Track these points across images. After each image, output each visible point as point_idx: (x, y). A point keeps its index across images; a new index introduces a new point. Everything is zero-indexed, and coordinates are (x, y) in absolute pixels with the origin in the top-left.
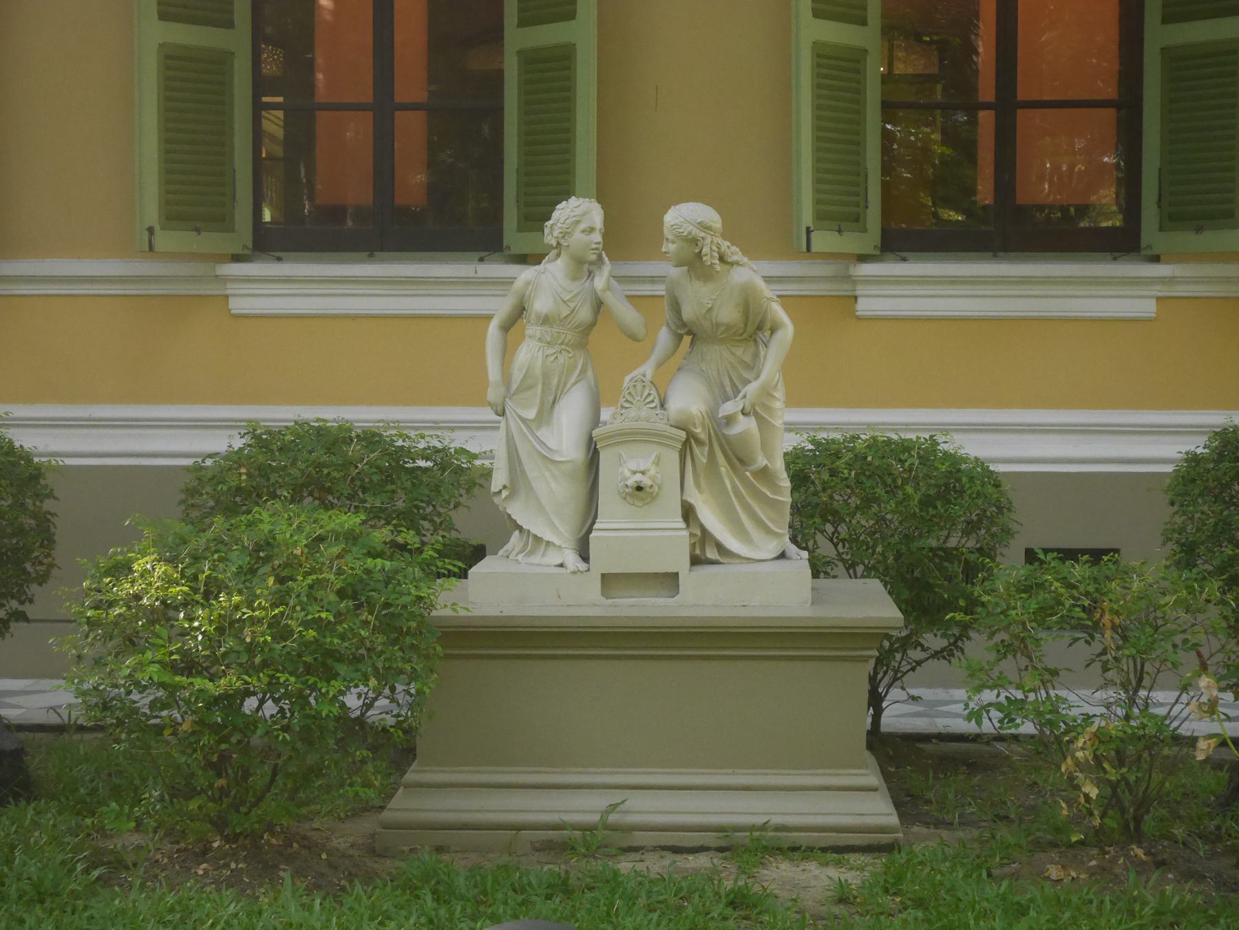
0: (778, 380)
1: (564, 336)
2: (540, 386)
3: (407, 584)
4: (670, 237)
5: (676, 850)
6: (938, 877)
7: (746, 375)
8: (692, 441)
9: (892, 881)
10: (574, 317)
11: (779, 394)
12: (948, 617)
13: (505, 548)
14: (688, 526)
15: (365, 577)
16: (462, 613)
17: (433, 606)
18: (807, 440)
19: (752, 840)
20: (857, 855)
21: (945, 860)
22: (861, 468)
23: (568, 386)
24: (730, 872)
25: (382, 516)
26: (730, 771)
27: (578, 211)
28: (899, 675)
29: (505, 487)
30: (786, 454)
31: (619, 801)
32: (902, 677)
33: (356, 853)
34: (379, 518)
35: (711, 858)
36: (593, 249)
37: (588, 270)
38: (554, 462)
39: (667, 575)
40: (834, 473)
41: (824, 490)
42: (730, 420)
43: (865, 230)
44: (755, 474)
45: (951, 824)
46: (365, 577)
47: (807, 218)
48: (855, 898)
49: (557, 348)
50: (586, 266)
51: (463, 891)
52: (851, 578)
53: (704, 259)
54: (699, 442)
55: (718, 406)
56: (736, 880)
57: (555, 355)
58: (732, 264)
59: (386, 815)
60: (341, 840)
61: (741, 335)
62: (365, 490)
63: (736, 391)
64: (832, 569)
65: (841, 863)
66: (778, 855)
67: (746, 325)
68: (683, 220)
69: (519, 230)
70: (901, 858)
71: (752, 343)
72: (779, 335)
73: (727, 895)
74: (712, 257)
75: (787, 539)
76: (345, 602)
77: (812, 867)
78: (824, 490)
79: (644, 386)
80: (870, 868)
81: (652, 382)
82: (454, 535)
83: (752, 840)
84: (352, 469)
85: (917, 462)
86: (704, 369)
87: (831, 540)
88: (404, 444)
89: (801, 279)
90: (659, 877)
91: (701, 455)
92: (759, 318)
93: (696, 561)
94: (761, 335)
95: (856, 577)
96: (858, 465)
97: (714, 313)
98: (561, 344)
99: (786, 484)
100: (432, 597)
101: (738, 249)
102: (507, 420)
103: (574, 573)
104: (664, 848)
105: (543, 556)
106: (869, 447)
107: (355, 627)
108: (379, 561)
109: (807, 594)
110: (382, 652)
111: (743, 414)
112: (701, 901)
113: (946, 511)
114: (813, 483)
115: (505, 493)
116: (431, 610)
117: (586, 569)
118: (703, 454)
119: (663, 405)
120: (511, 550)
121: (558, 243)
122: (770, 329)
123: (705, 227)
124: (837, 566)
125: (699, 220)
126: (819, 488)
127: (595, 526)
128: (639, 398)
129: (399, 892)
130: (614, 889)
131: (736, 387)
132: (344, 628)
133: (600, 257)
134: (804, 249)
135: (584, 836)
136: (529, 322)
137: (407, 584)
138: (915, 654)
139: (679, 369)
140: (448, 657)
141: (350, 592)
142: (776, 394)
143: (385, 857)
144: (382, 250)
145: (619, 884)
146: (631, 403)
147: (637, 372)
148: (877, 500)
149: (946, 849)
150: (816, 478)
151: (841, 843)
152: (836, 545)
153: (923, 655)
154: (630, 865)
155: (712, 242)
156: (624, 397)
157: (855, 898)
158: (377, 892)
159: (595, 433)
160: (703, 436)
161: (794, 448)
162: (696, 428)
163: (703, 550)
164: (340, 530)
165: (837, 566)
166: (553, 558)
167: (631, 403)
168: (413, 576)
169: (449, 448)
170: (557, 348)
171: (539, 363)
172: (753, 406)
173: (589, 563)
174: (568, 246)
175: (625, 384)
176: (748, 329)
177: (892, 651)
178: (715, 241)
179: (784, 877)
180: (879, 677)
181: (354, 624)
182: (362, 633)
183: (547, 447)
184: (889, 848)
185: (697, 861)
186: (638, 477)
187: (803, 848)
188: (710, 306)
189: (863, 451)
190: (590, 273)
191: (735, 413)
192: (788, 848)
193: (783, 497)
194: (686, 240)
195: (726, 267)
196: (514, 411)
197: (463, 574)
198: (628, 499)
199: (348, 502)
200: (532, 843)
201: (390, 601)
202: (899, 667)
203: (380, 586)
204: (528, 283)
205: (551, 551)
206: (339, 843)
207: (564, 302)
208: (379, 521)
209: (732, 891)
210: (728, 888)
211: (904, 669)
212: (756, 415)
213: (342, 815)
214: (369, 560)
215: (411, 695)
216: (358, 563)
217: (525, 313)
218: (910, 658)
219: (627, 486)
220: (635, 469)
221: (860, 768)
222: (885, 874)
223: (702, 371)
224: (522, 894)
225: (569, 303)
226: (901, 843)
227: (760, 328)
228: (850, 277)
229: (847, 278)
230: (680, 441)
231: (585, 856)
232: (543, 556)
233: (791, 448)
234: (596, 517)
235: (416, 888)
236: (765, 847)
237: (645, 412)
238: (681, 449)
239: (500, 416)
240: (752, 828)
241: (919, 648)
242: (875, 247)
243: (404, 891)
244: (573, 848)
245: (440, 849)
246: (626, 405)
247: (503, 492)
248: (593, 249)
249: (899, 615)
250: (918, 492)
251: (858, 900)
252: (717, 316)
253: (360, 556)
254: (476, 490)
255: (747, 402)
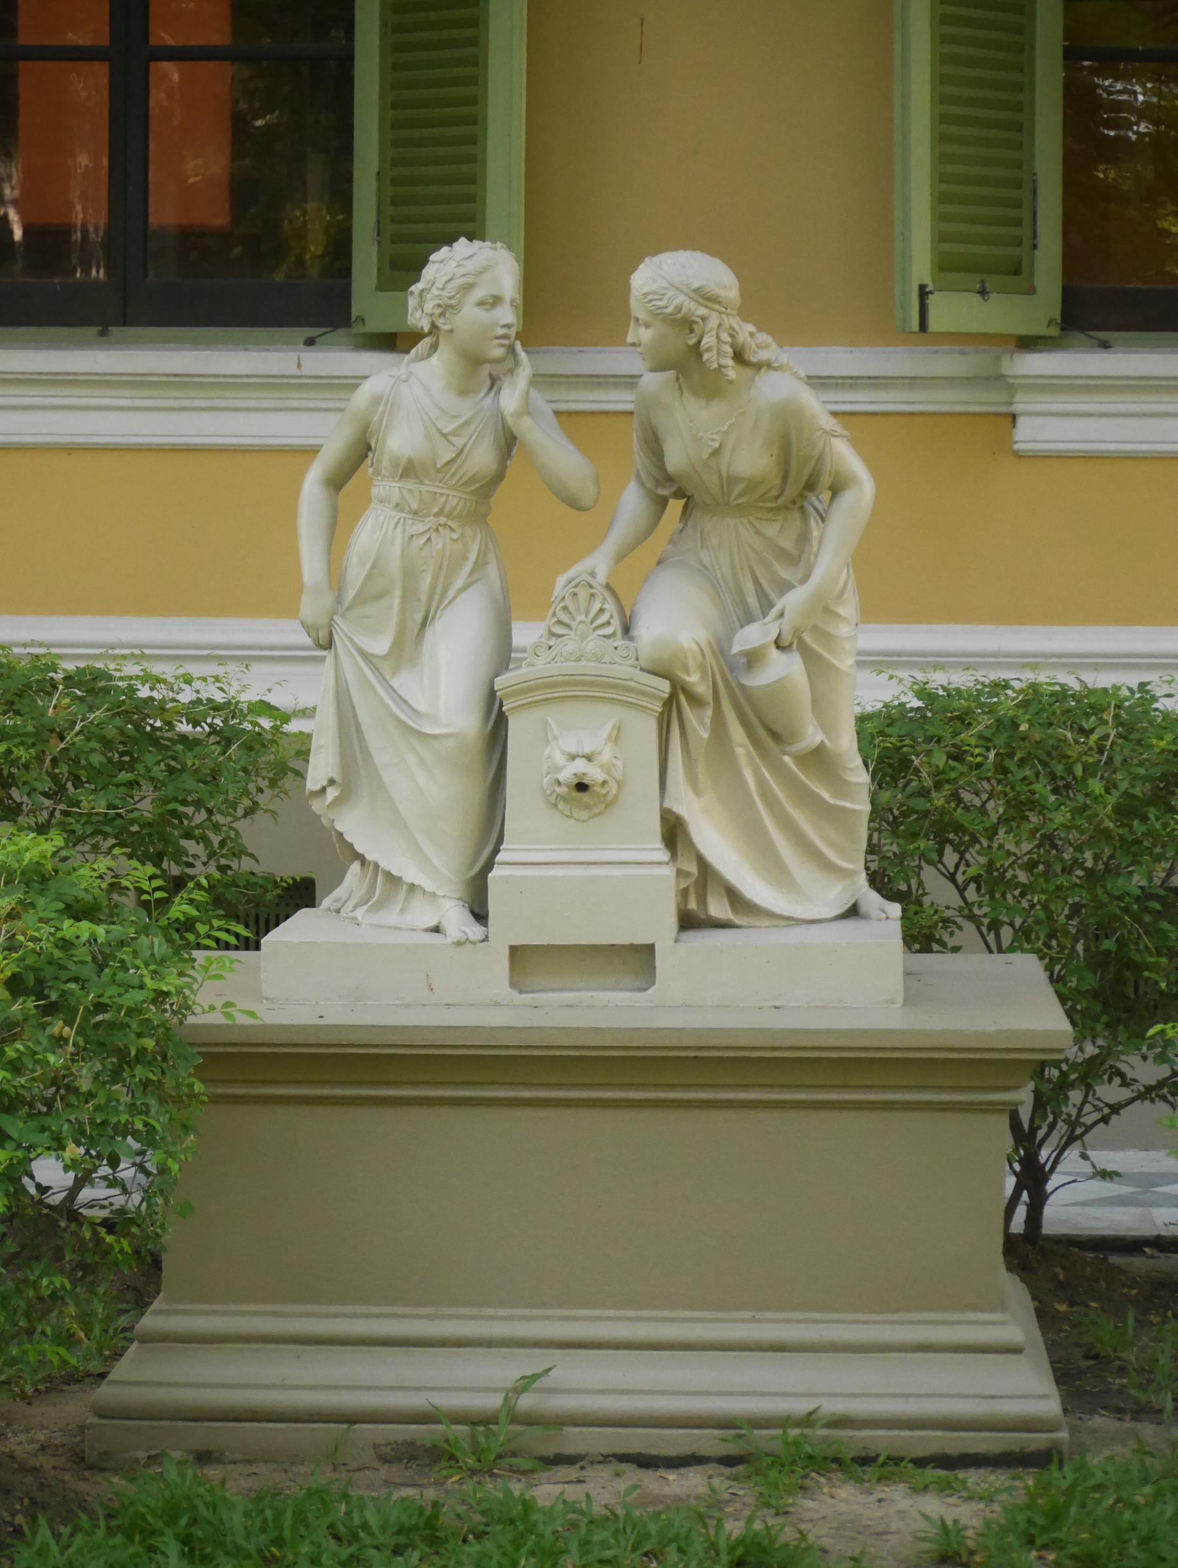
0: (846, 584)
1: (443, 499)
2: (397, 594)
3: (138, 968)
4: (642, 316)
5: (646, 1462)
6: (1127, 1515)
7: (785, 574)
8: (682, 698)
9: (1040, 1521)
10: (465, 460)
11: (848, 609)
12: (1151, 1032)
13: (336, 893)
14: (674, 856)
15: (58, 954)
16: (243, 1020)
17: (188, 1008)
18: (911, 689)
19: (787, 1444)
20: (982, 1471)
21: (1145, 1481)
22: (1009, 745)
23: (447, 601)
24: (744, 1504)
25: (108, 829)
26: (747, 1315)
27: (470, 266)
28: (1078, 1131)
29: (332, 782)
30: (862, 719)
31: (539, 1370)
32: (1083, 1134)
33: (46, 1462)
34: (106, 836)
35: (710, 1477)
36: (498, 338)
37: (491, 376)
38: (422, 736)
39: (633, 948)
40: (957, 756)
41: (938, 785)
42: (753, 659)
43: (1032, 291)
44: (802, 759)
45: (1161, 1411)
46: (58, 954)
47: (921, 269)
48: (972, 1553)
49: (431, 522)
50: (486, 369)
51: (240, 1540)
52: (991, 952)
53: (706, 356)
54: (696, 701)
55: (731, 632)
56: (750, 1520)
57: (427, 536)
58: (758, 366)
59: (105, 1393)
60: (22, 1437)
61: (777, 498)
62: (78, 782)
63: (767, 605)
64: (952, 934)
65: (952, 1488)
66: (834, 1471)
67: (785, 478)
68: (665, 284)
69: (381, 287)
70: (1061, 1477)
71: (797, 515)
72: (847, 499)
73: (732, 1549)
74: (720, 353)
75: (862, 880)
76: (21, 1000)
77: (897, 1495)
78: (938, 785)
79: (592, 595)
80: (1004, 1497)
81: (608, 587)
82: (246, 864)
83: (787, 1444)
84: (54, 741)
85: (1113, 733)
86: (706, 561)
87: (952, 878)
88: (155, 694)
89: (912, 382)
90: (608, 1513)
91: (699, 724)
92: (807, 472)
93: (689, 922)
94: (814, 499)
95: (1000, 950)
96: (1001, 739)
97: (726, 457)
98: (439, 513)
99: (861, 777)
100: (187, 992)
101: (769, 339)
102: (336, 656)
103: (459, 944)
104: (623, 1458)
105: (403, 910)
106: (1025, 704)
107: (38, 1049)
108: (85, 924)
109: (894, 984)
110: (91, 1095)
111: (778, 647)
112: (681, 1560)
113: (1165, 826)
114: (917, 771)
115: (332, 793)
116: (185, 1016)
117: (481, 937)
118: (702, 723)
119: (627, 630)
120: (344, 897)
121: (434, 326)
122: (830, 488)
123: (707, 298)
124: (960, 928)
125: (696, 285)
126: (928, 782)
127: (500, 858)
128: (582, 617)
129: (118, 1540)
130: (522, 1535)
131: (767, 597)
132: (17, 1051)
133: (511, 350)
134: (915, 325)
135: (473, 1436)
136: (377, 472)
137: (138, 968)
138: (1110, 1092)
139: (659, 563)
140: (216, 1100)
141: (30, 981)
142: (841, 610)
143: (102, 1470)
144: (124, 324)
145: (532, 1528)
146: (567, 626)
147: (578, 570)
148: (1033, 803)
149: (1148, 1460)
150: (922, 763)
151: (953, 1450)
152: (961, 891)
153: (1125, 1094)
154: (556, 1489)
155: (720, 326)
156: (554, 614)
157: (972, 1553)
158: (79, 1540)
159: (499, 683)
160: (702, 689)
161: (886, 706)
162: (689, 674)
163: (703, 900)
164: (15, 865)
165: (960, 928)
166: (422, 915)
167: (567, 626)
168: (149, 953)
169: (238, 703)
170: (431, 522)
171: (397, 551)
172: (796, 632)
173: (486, 925)
174: (452, 331)
175: (557, 591)
176: (788, 488)
177: (1063, 1086)
178: (727, 325)
179: (841, 1514)
180: (1040, 1134)
181: (39, 1043)
182: (52, 1059)
183: (413, 710)
184: (1039, 1460)
185: (684, 1482)
186: (580, 766)
187: (881, 1459)
188: (717, 445)
189: (1011, 713)
190: (494, 381)
191: (763, 647)
192: (854, 1460)
193: (853, 801)
194: (673, 321)
195: (747, 372)
196: (351, 640)
197: (253, 945)
198: (561, 806)
199: (48, 803)
200: (375, 1446)
201: (105, 1000)
202: (1079, 1116)
203: (88, 971)
204: (376, 401)
205: (418, 903)
206: (20, 1444)
207: (444, 436)
208: (105, 839)
209: (741, 1541)
210: (734, 1536)
211: (1088, 1120)
212: (804, 649)
213: (29, 1389)
214: (67, 923)
215: (148, 1174)
216: (47, 929)
217: (370, 455)
218: (1099, 1099)
219: (559, 783)
220: (573, 751)
221: (992, 1310)
222: (1029, 1507)
223: (704, 566)
224: (350, 1544)
225: (452, 438)
226: (1065, 1450)
227: (810, 486)
228: (1003, 377)
229: (997, 380)
230: (659, 698)
231: (474, 1472)
232: (403, 910)
233: (879, 705)
234: (500, 840)
235: (153, 1532)
236: (810, 1457)
237: (592, 644)
238: (662, 714)
239: (325, 649)
240: (785, 1422)
241: (1117, 1081)
242: (1050, 322)
243: (129, 1538)
244: (452, 1457)
245: (204, 1457)
246: (559, 630)
247: (328, 790)
248: (498, 338)
249: (1064, 1025)
250: (1113, 791)
251: (977, 1558)
252: (729, 466)
253: (52, 915)
254: (288, 781)
255: (787, 626)
